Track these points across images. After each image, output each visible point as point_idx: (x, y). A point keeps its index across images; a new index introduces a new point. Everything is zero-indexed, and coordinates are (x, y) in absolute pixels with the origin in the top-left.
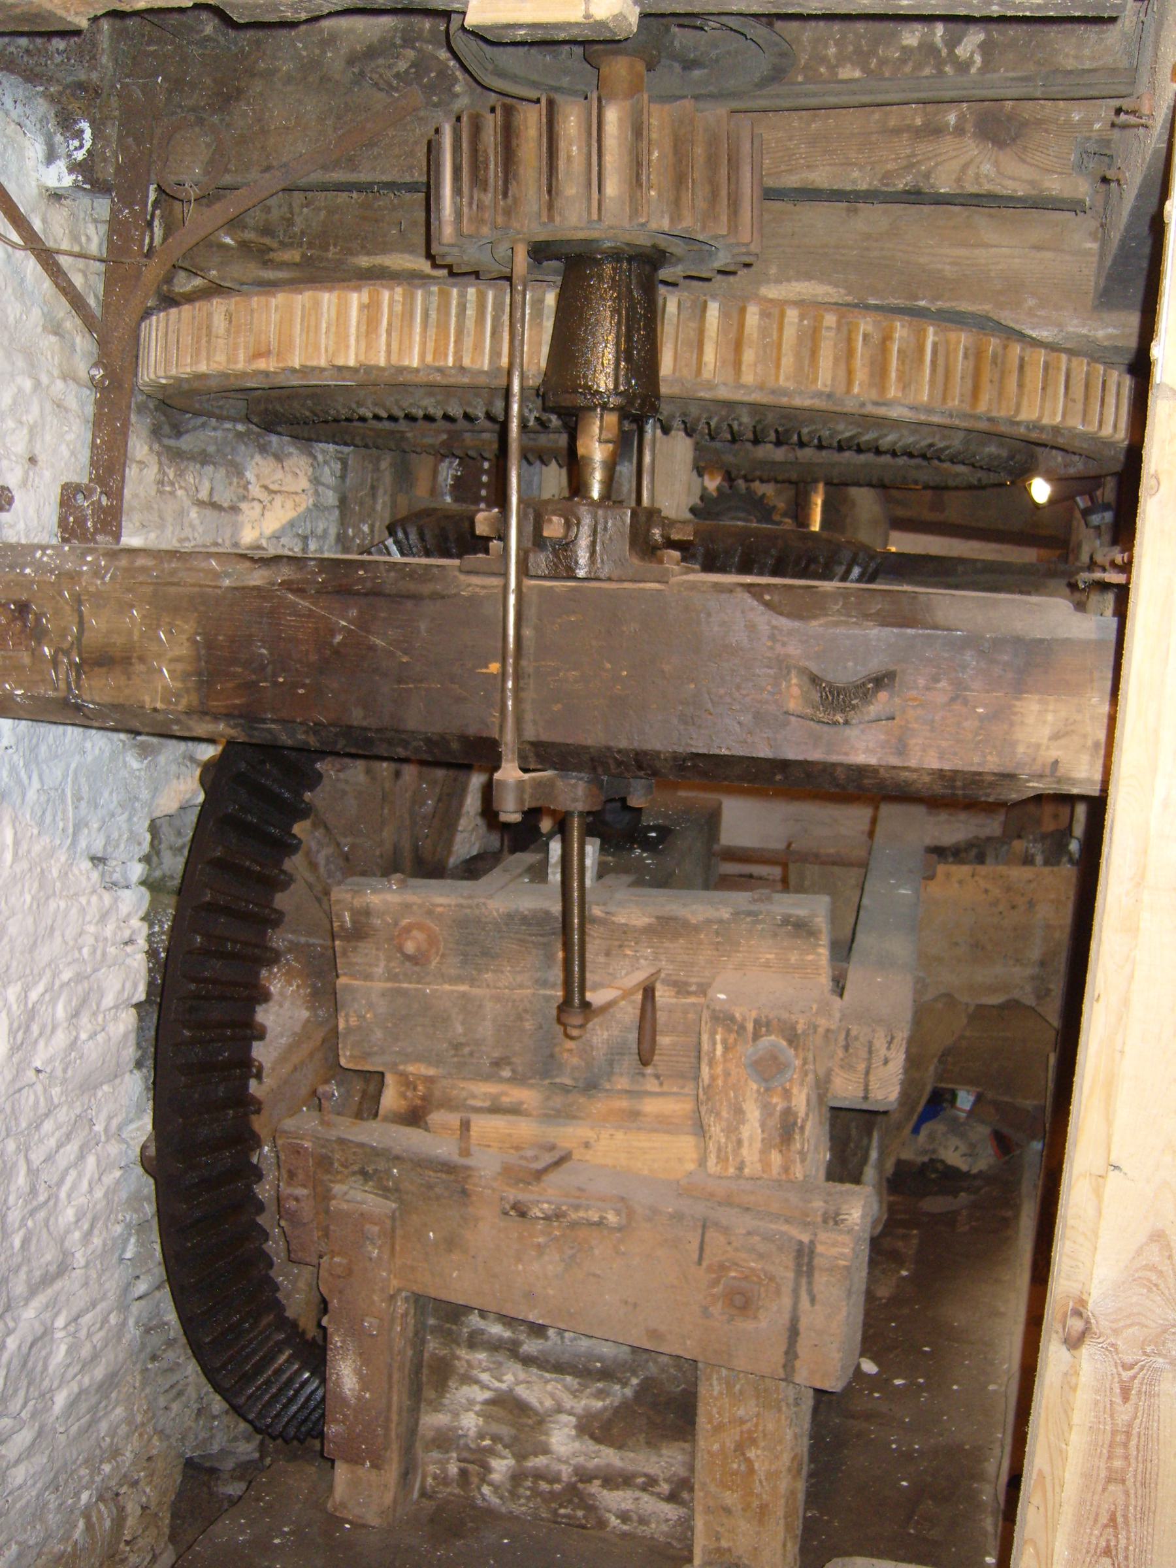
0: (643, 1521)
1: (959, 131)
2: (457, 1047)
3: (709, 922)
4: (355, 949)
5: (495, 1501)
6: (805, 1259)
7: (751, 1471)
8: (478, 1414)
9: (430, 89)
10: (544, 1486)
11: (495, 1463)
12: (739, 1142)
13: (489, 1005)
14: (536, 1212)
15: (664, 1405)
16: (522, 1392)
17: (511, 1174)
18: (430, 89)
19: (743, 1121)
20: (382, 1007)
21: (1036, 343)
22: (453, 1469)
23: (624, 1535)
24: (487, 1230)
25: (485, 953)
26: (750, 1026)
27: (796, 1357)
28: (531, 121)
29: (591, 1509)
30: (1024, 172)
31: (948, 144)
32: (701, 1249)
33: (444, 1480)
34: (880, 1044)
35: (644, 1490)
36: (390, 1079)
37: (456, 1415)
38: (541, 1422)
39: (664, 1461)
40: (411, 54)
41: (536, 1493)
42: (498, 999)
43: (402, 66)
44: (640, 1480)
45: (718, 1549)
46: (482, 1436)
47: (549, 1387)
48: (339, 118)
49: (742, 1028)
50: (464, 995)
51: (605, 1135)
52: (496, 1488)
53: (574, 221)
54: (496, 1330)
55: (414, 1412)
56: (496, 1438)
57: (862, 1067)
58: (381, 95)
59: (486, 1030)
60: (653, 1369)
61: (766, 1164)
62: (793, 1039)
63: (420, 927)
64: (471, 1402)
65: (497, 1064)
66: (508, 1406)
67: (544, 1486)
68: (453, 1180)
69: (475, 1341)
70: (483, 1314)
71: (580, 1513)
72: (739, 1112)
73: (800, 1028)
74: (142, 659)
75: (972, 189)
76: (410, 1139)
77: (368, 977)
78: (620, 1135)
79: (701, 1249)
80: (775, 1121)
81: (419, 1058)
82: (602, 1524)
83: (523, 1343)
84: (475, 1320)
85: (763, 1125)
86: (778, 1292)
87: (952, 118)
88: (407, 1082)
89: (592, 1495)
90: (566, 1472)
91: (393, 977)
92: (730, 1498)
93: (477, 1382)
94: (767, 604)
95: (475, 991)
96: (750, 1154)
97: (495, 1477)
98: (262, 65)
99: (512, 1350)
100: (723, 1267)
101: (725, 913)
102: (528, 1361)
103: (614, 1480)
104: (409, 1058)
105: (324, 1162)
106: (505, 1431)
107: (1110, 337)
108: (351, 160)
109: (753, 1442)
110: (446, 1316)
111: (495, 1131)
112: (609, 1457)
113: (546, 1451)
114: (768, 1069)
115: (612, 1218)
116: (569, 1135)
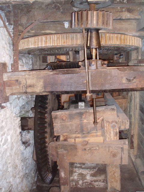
0: (100, 185)
1: (125, 11)
2: (70, 130)
3: (102, 110)
4: (56, 120)
5: (80, 187)
6: (122, 148)
7: (115, 176)
8: (77, 176)
9: (57, 9)
10: (86, 184)
11: (80, 182)
12: (111, 136)
13: (74, 125)
14: (87, 149)
15: (101, 170)
16: (83, 172)
17: (83, 145)
18: (57, 9)
19: (111, 134)
20: (60, 127)
21: (130, 36)
22: (74, 184)
23: (97, 188)
24: (80, 152)
25: (73, 118)
26: (111, 122)
27: (122, 161)
28: (85, 13)
29: (93, 185)
30: (133, 16)
31: (124, 13)
32: (109, 150)
33: (73, 186)
34: (126, 122)
35: (99, 181)
36: (61, 136)
37: (74, 177)
38: (85, 176)
39: (102, 177)
40: (54, 5)
41: (85, 185)
42: (75, 124)
43: (53, 6)
44: (99, 180)
45: (112, 187)
46: (78, 179)
47: (86, 171)
48: (45, 13)
49: (110, 122)
50: (71, 124)
51: (91, 138)
52: (80, 185)
53: (89, 26)
54: (78, 165)
55: (70, 177)
56: (79, 179)
57: (124, 125)
58: (50, 10)
59: (74, 128)
60: (99, 166)
61: (114, 139)
62: (116, 123)
63: (64, 116)
64: (76, 175)
65: (76, 132)
66: (81, 175)
67: (86, 184)
68: (74, 147)
69: (76, 167)
70: (76, 164)
71: (92, 186)
72: (110, 133)
73: (117, 121)
74: (36, 86)
75: (127, 18)
76: (66, 143)
77: (58, 123)
78: (93, 138)
79: (109, 150)
80: (115, 133)
81: (65, 133)
82: (94, 187)
83: (82, 165)
84: (75, 165)
85: (113, 134)
86: (119, 154)
87: (124, 10)
88: (64, 136)
89: (93, 184)
90: (89, 181)
91: (61, 123)
92: (113, 180)
93: (77, 172)
94: (119, 70)
95: (72, 123)
96: (112, 138)
97: (80, 184)
98: (34, 7)
99: (81, 167)
100: (112, 152)
101: (104, 109)
102: (83, 168)
103: (95, 181)
104: (64, 133)
105: (56, 148)
106: (81, 178)
107: (138, 35)
108: (47, 19)
109: (115, 173)
110: (72, 164)
111: (78, 140)
112: (95, 178)
113: (86, 179)
114: (114, 127)
115: (97, 148)
116: (87, 139)
